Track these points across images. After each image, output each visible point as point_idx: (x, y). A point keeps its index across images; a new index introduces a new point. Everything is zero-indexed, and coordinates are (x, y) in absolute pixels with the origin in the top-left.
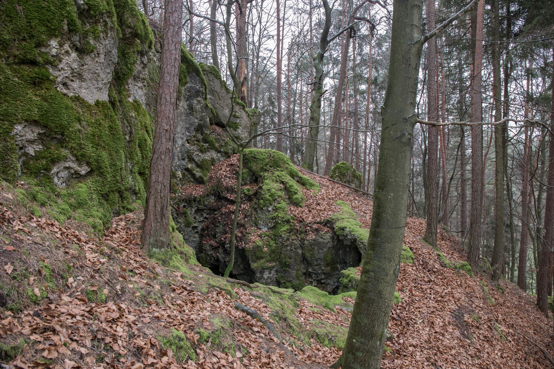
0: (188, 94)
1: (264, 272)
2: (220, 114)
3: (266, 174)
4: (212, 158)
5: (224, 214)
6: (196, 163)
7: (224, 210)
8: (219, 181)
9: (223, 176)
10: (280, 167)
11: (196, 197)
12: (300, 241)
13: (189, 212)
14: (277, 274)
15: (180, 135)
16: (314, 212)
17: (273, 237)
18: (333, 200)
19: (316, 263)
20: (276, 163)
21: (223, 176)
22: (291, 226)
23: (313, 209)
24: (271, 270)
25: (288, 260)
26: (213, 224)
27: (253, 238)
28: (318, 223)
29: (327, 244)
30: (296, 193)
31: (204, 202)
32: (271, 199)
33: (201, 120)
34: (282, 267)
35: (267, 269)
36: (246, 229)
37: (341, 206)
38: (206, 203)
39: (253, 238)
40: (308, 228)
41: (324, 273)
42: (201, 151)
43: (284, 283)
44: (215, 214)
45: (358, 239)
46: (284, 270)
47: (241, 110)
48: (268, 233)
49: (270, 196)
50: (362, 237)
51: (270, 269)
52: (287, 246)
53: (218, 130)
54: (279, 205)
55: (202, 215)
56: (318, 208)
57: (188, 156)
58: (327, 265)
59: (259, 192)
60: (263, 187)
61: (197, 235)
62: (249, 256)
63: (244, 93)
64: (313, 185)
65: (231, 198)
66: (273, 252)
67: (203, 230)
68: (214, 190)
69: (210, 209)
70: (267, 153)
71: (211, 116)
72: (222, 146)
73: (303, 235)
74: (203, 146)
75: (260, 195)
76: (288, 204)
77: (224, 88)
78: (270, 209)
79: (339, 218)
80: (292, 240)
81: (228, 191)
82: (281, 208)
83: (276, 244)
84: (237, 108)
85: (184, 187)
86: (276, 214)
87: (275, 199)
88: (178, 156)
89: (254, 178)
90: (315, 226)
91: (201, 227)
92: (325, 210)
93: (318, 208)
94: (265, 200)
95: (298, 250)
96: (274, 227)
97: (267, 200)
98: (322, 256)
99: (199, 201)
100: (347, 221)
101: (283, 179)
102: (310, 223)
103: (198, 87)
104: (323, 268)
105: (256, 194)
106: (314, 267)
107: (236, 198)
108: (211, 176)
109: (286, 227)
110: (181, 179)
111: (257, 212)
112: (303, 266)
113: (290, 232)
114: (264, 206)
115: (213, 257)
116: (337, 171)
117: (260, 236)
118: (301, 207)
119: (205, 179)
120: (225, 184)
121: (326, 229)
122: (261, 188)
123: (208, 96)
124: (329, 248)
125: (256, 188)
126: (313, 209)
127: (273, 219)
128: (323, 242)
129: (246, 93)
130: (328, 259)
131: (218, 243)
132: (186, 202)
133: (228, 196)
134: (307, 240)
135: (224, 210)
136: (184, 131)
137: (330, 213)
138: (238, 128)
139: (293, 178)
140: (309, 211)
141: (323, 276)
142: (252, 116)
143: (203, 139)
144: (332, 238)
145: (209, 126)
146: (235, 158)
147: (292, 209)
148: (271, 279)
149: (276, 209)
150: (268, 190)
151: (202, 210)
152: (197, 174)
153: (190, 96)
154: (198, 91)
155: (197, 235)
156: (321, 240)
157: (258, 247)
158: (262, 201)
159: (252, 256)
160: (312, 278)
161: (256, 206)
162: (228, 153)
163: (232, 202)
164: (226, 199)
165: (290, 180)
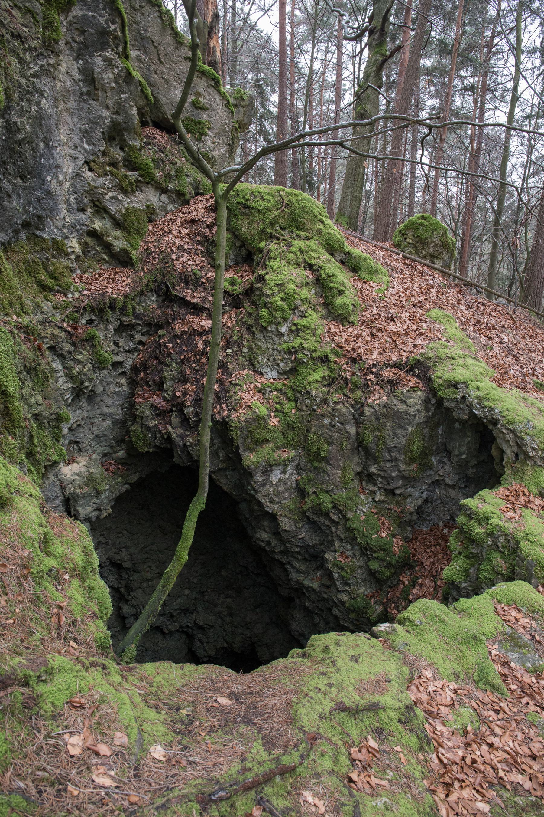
0: (79, 39)
1: (271, 471)
2: (163, 100)
3: (272, 246)
4: (148, 207)
5: (180, 337)
6: (112, 218)
7: (178, 327)
8: (166, 261)
9: (175, 249)
10: (304, 229)
11: (115, 300)
12: (352, 406)
13: (100, 335)
14: (299, 474)
15: (67, 150)
16: (384, 337)
17: (289, 393)
18: (421, 307)
19: (387, 456)
20: (295, 220)
21: (175, 249)
22: (331, 370)
23: (380, 330)
24: (286, 465)
25: (326, 447)
26: (156, 358)
27: (246, 396)
28: (394, 366)
29: (415, 416)
30: (341, 293)
31: (134, 308)
32: (286, 307)
33: (117, 113)
34: (311, 461)
35: (277, 465)
36: (229, 374)
37: (440, 323)
38: (140, 310)
39: (246, 396)
40: (372, 377)
41: (403, 477)
42: (123, 190)
43: (315, 493)
44: (160, 337)
45: (502, 421)
46: (316, 468)
47: (211, 90)
48: (279, 384)
49: (282, 299)
50: (511, 415)
51: (284, 464)
52: (323, 416)
53: (161, 138)
54: (304, 322)
55: (132, 337)
56: (391, 327)
57: (92, 201)
58: (411, 461)
59: (258, 289)
60: (267, 277)
61: (123, 381)
62: (237, 436)
63: (214, 54)
64: (376, 272)
65: (195, 301)
66: (291, 427)
67: (135, 369)
68: (155, 281)
69: (149, 325)
70: (273, 196)
71: (142, 102)
72: (170, 177)
73: (359, 393)
74: (126, 176)
75: (260, 296)
76: (323, 317)
77: (169, 32)
78: (283, 330)
79: (443, 356)
80: (335, 403)
81: (187, 283)
82: (308, 328)
83: (298, 410)
84: (201, 84)
85: (88, 275)
86: (296, 343)
87: (296, 308)
88: (68, 202)
89: (244, 252)
90: (388, 373)
91: (130, 362)
92: (407, 334)
93: (391, 327)
94: (272, 309)
95: (348, 427)
96: (293, 371)
97: (276, 310)
98: (404, 441)
99: (123, 309)
100: (464, 366)
101: (312, 258)
102: (374, 365)
103: (102, 20)
104: (402, 467)
105: (249, 291)
106: (382, 464)
107: (204, 299)
108: (148, 248)
109: (320, 373)
110: (78, 257)
111: (253, 334)
112: (356, 459)
113: (329, 385)
114: (271, 323)
115: (160, 432)
116: (410, 234)
117: (261, 391)
118: (352, 323)
119: (135, 254)
120: (179, 267)
121: (413, 381)
122: (261, 279)
123: (133, 53)
124: (419, 424)
125: (249, 278)
126: (380, 330)
127: (289, 352)
128: (407, 413)
129: (218, 53)
130: (414, 448)
131: (168, 401)
132: (92, 311)
133: (188, 294)
134: (370, 406)
135: (178, 327)
136: (76, 139)
137: (419, 341)
138: (206, 134)
139: (332, 255)
140: (372, 335)
141: (400, 483)
142: (236, 106)
143: (124, 160)
144: (426, 402)
145: (139, 130)
146: (200, 206)
147: (333, 330)
148: (285, 484)
149: (297, 331)
150: (277, 285)
151: (132, 327)
152: (116, 243)
153: (84, 46)
154: (104, 33)
155: (123, 381)
156: (401, 407)
157: (258, 418)
158: (264, 312)
159: (246, 439)
160: (375, 484)
161: (251, 322)
162: (183, 194)
163: (197, 309)
164: (184, 302)
165: (329, 261)
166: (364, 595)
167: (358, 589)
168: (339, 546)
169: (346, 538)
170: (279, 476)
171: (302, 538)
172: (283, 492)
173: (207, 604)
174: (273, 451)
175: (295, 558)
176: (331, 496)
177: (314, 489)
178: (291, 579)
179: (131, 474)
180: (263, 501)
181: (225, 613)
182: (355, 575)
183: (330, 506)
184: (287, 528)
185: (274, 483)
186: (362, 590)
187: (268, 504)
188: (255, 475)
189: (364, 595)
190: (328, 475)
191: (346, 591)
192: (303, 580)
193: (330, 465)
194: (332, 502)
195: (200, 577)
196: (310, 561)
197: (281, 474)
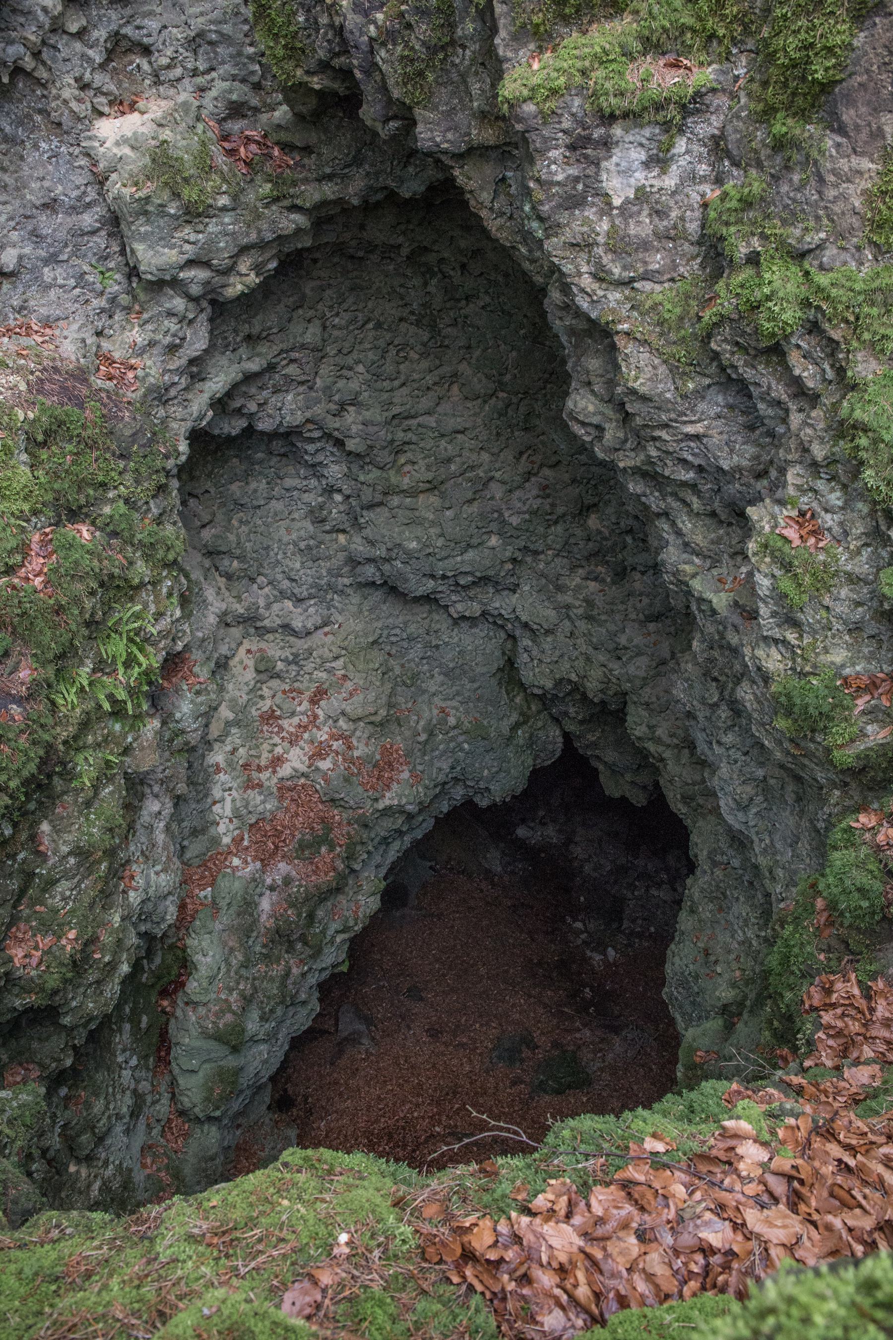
1: (607, 144)
148: (659, 213)
166: (838, 675)
167: (826, 651)
168: (798, 487)
169: (832, 461)
170: (640, 176)
171: (697, 437)
172: (645, 246)
173: (544, 581)
174: (628, 54)
175: (684, 502)
176: (807, 273)
177: (756, 243)
178: (663, 563)
179: (306, 181)
180: (568, 268)
181: (580, 611)
182: (827, 601)
183: (790, 315)
184: (640, 384)
185: (617, 202)
186: (838, 656)
187: (587, 281)
188: (542, 152)
189: (838, 675)
190: (821, 180)
191: (784, 642)
192: (694, 576)
193: (841, 130)
194: (806, 304)
195: (527, 516)
196: (730, 524)
197: (647, 165)
